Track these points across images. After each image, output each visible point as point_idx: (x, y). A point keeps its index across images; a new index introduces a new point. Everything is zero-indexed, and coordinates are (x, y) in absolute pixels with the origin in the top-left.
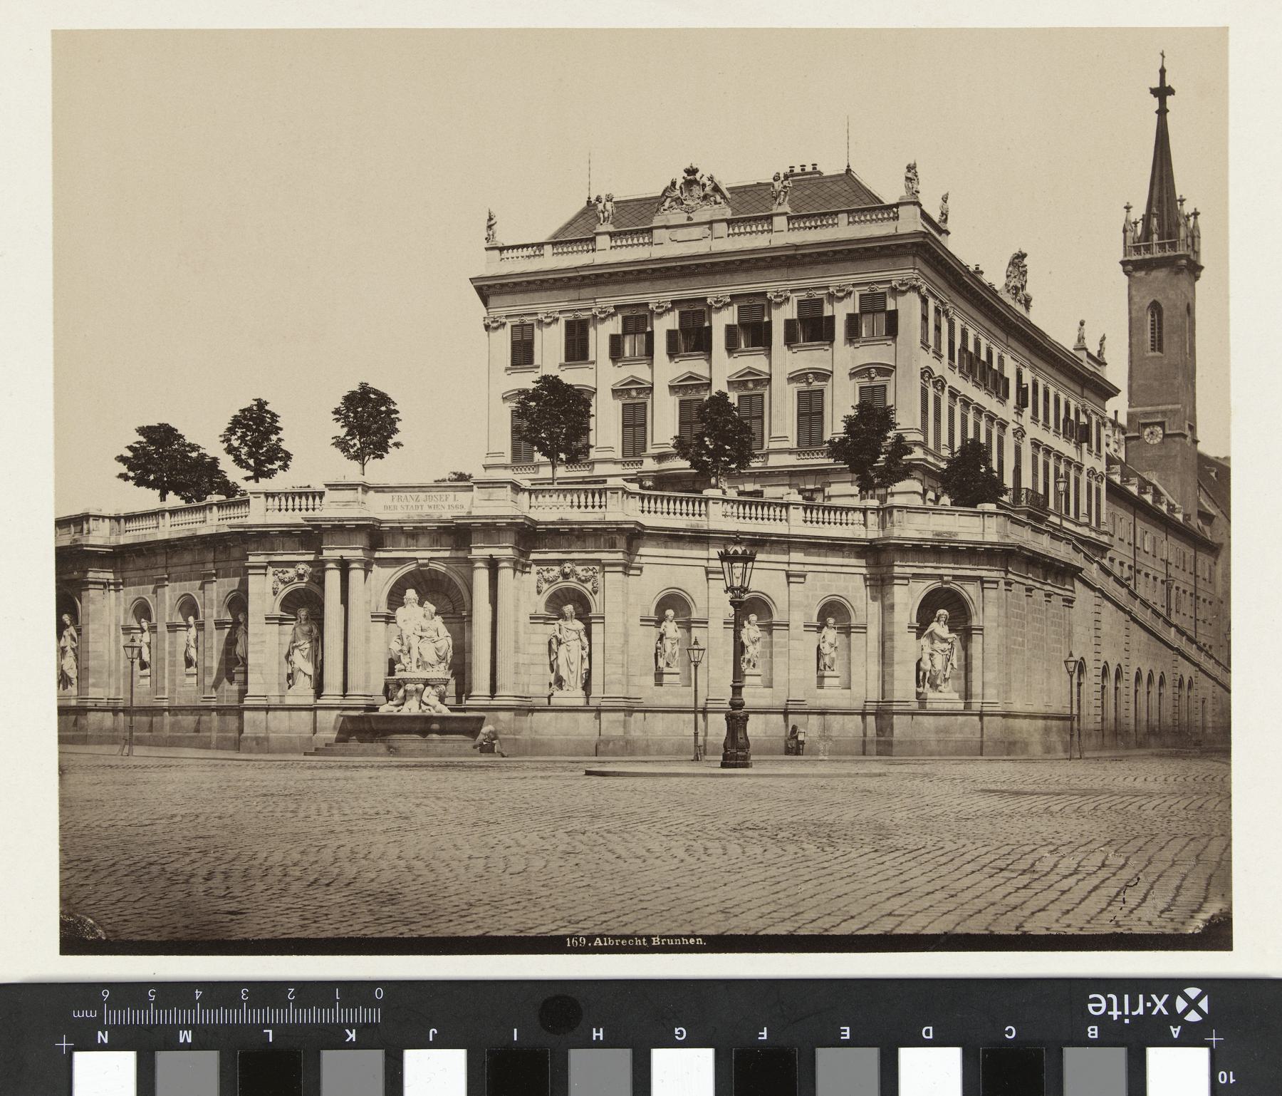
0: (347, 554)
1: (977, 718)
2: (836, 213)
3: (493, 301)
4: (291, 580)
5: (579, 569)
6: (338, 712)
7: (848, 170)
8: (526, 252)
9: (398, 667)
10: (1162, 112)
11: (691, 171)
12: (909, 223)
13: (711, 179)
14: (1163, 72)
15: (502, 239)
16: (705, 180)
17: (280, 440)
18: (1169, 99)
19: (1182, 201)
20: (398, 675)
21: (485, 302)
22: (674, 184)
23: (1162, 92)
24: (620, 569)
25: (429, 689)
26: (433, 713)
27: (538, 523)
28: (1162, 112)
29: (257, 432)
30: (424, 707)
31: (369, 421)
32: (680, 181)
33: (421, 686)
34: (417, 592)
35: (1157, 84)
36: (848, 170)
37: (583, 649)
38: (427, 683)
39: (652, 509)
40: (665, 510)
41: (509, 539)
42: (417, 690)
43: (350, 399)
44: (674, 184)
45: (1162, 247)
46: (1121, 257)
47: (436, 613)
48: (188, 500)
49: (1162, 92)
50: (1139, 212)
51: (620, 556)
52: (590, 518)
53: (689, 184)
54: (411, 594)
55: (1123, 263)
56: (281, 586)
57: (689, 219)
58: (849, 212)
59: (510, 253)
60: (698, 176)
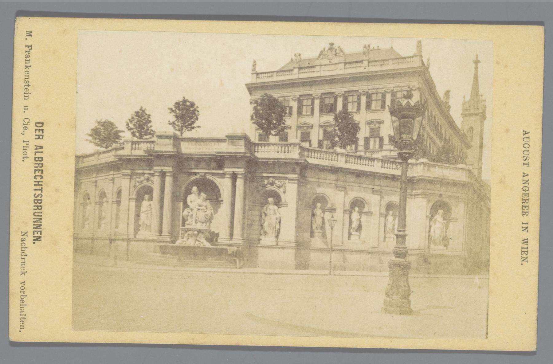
0: (166, 169)
1: (90, 241)
2: (388, 60)
3: (253, 93)
4: (142, 181)
5: (277, 182)
6: (156, 244)
7: (392, 48)
8: (268, 75)
9: (187, 223)
10: (476, 68)
11: (332, 44)
12: (416, 63)
13: (339, 47)
14: (477, 56)
15: (259, 70)
16: (336, 48)
17: (151, 126)
18: (479, 65)
19: (482, 95)
20: (187, 227)
21: (250, 93)
22: (324, 49)
23: (477, 62)
24: (296, 182)
25: (200, 234)
26: (202, 245)
27: (258, 158)
28: (476, 68)
29: (141, 123)
30: (197, 243)
31: (186, 113)
32: (327, 49)
33: (196, 232)
34: (198, 187)
35: (475, 59)
36: (392, 48)
37: (277, 219)
38: (199, 231)
39: (313, 156)
40: (319, 157)
41: (243, 163)
42: (194, 234)
43: (177, 104)
44: (324, 49)
45: (474, 109)
46: (461, 112)
47: (207, 199)
48: (106, 147)
49: (477, 62)
50: (468, 98)
51: (296, 176)
52: (283, 157)
53: (330, 49)
54: (195, 188)
55: (462, 114)
56: (137, 184)
57: (330, 62)
58: (392, 59)
59: (261, 76)
60: (334, 46)
